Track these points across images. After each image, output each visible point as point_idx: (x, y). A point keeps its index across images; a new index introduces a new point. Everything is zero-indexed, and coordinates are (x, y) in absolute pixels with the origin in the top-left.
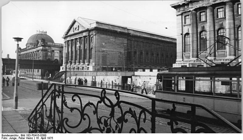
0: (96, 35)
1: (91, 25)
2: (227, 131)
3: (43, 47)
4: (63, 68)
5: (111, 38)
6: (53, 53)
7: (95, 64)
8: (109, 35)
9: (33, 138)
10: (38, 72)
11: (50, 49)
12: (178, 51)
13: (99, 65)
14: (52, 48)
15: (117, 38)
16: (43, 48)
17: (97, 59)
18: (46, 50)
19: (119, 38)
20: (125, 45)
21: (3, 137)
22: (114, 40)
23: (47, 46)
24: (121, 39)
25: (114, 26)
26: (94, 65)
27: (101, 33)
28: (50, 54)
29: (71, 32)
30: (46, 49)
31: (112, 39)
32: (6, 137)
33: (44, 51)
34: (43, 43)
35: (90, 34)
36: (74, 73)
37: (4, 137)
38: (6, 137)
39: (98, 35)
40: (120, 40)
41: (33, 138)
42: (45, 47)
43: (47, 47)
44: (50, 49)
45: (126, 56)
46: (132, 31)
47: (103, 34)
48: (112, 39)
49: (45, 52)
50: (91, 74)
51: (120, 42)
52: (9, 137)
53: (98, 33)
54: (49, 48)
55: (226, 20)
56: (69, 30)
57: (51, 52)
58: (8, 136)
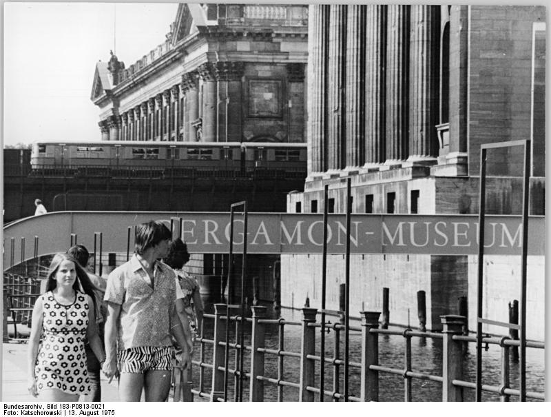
2: (436, 399)
6: (294, 88)
7: (463, 163)
9: (63, 413)
10: (299, 205)
11: (269, 58)
12: (516, 141)
14: (285, 47)
18: (236, 70)
21: (7, 409)
23: (239, 36)
26: (453, 172)
28: (269, 96)
30: (233, 58)
32: (13, 410)
33: (223, 79)
37: (10, 410)
38: (13, 410)
41: (63, 413)
42: (230, 45)
43: (243, 46)
44: (269, 58)
49: (226, 85)
50: (304, 233)
52: (18, 411)
54: (263, 45)
55: (307, 41)
57: (275, 78)
58: (19, 407)
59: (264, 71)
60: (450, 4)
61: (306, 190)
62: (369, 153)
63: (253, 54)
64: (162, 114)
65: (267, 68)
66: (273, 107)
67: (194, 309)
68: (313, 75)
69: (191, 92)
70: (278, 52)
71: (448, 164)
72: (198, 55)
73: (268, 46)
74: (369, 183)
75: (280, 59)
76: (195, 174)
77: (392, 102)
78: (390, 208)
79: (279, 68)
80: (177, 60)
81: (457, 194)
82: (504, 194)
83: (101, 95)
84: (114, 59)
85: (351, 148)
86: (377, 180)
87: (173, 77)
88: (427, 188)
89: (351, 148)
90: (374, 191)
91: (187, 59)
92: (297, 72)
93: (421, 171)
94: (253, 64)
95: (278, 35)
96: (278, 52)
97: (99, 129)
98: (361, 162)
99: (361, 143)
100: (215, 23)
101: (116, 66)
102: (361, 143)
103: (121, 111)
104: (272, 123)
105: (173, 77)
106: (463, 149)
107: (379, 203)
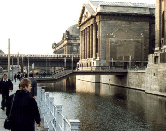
0: (101, 21)
1: (97, 9)
3: (67, 40)
4: (156, 58)
5: (124, 24)
7: (100, 59)
8: (120, 20)
11: (75, 43)
13: (105, 59)
15: (132, 23)
16: (67, 42)
17: (103, 52)
19: (136, 23)
20: (146, 32)
22: (128, 26)
24: (139, 23)
25: (127, 7)
27: (107, 19)
28: (76, 48)
29: (83, 21)
30: (70, 43)
31: (125, 24)
34: (67, 37)
35: (95, 22)
36: (82, 68)
39: (103, 21)
40: (137, 25)
43: (72, 41)
44: (75, 43)
45: (148, 46)
46: (123, 8)
47: (111, 19)
48: (124, 24)
51: (137, 28)
53: (103, 19)
54: (75, 41)
56: (81, 18)
59: (75, 45)
60: (9, 38)
61: (80, 62)
62: (85, 58)
63: (160, 38)
64: (61, 51)
65: (75, 44)
66: (76, 50)
67: (35, 80)
68: (81, 45)
69: (65, 47)
70: (77, 42)
71: (98, 59)
72: (66, 42)
73: (76, 41)
74: (87, 61)
75: (77, 43)
76: (156, 54)
77: (91, 49)
78: (90, 65)
79: (77, 44)
80: (63, 43)
81: (99, 63)
82: (48, 66)
83: (53, 48)
84: (55, 43)
85: (85, 56)
86: (88, 61)
87: (63, 44)
88: (95, 62)
89: (85, 56)
90: (88, 63)
91: (64, 43)
92: (79, 44)
93: (94, 59)
94: (73, 43)
95: (77, 39)
96: (77, 42)
97: (53, 53)
98: (86, 58)
99: (87, 55)
100: (68, 38)
101: (55, 44)
102: (87, 55)
103: (56, 50)
104: (76, 52)
105: (63, 44)
106: (100, 57)
107: (89, 64)
